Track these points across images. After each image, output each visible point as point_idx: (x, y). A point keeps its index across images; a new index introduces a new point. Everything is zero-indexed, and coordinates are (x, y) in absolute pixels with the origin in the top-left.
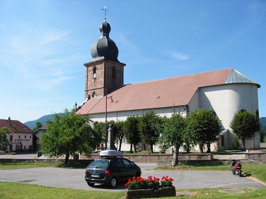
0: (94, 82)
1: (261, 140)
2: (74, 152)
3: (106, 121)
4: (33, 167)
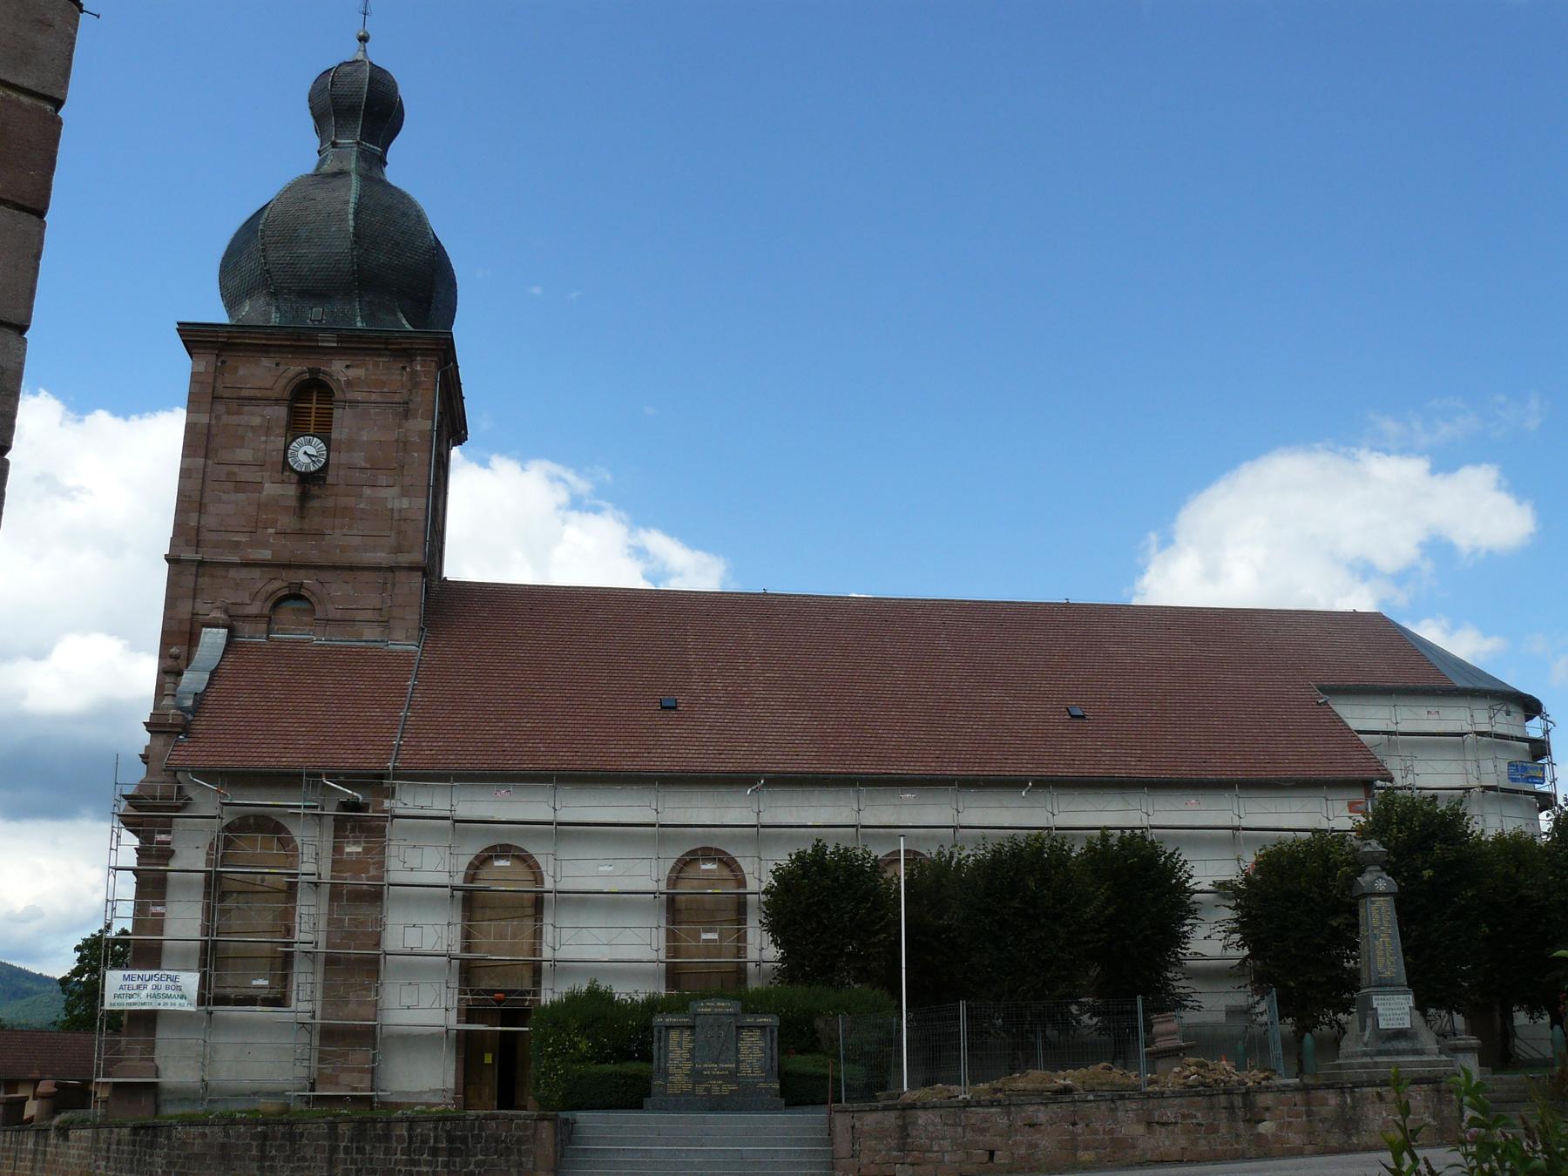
0: (294, 503)
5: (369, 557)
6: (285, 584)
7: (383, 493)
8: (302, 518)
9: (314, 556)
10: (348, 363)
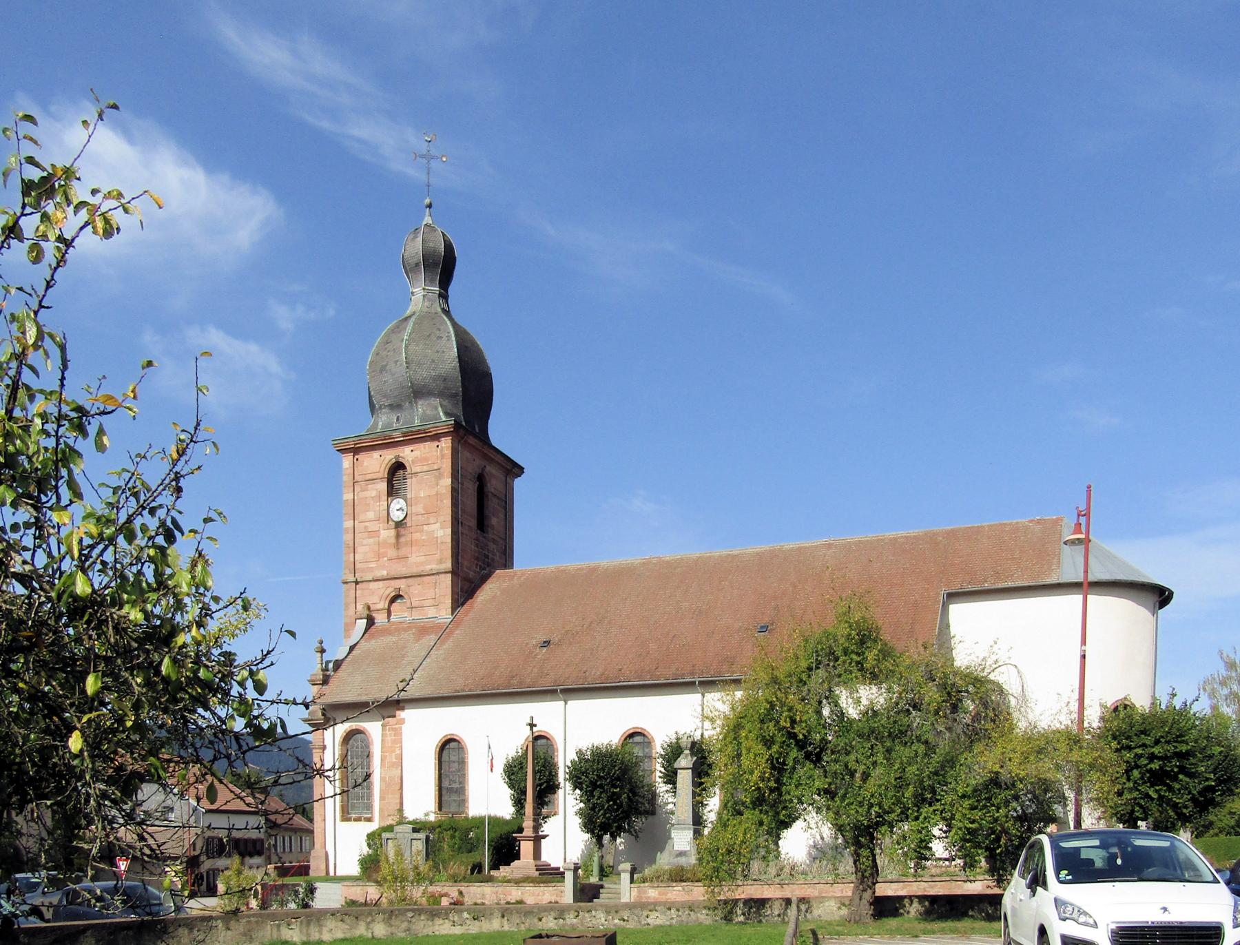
0: (393, 541)
1: (351, 900)
2: (1018, 815)
3: (703, 696)
4: (934, 933)
5: (428, 568)
6: (393, 589)
7: (433, 527)
8: (398, 549)
9: (404, 571)
10: (412, 448)
